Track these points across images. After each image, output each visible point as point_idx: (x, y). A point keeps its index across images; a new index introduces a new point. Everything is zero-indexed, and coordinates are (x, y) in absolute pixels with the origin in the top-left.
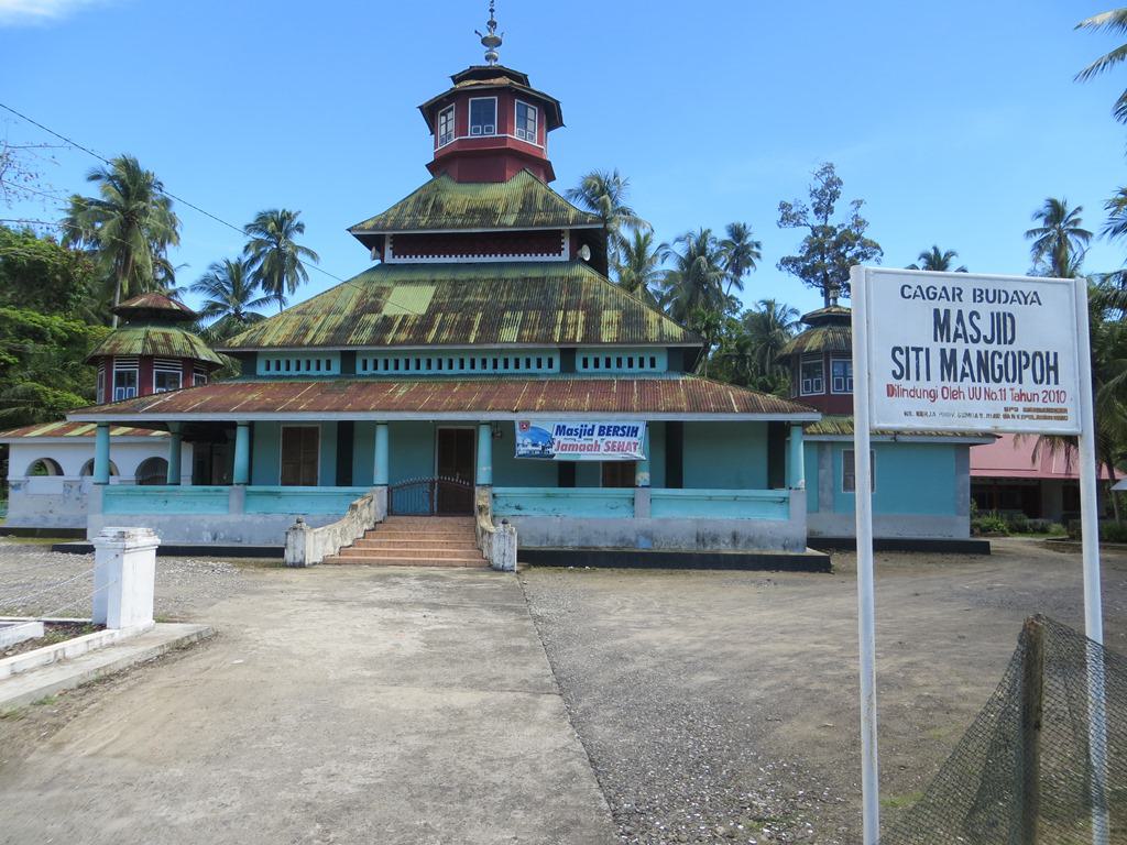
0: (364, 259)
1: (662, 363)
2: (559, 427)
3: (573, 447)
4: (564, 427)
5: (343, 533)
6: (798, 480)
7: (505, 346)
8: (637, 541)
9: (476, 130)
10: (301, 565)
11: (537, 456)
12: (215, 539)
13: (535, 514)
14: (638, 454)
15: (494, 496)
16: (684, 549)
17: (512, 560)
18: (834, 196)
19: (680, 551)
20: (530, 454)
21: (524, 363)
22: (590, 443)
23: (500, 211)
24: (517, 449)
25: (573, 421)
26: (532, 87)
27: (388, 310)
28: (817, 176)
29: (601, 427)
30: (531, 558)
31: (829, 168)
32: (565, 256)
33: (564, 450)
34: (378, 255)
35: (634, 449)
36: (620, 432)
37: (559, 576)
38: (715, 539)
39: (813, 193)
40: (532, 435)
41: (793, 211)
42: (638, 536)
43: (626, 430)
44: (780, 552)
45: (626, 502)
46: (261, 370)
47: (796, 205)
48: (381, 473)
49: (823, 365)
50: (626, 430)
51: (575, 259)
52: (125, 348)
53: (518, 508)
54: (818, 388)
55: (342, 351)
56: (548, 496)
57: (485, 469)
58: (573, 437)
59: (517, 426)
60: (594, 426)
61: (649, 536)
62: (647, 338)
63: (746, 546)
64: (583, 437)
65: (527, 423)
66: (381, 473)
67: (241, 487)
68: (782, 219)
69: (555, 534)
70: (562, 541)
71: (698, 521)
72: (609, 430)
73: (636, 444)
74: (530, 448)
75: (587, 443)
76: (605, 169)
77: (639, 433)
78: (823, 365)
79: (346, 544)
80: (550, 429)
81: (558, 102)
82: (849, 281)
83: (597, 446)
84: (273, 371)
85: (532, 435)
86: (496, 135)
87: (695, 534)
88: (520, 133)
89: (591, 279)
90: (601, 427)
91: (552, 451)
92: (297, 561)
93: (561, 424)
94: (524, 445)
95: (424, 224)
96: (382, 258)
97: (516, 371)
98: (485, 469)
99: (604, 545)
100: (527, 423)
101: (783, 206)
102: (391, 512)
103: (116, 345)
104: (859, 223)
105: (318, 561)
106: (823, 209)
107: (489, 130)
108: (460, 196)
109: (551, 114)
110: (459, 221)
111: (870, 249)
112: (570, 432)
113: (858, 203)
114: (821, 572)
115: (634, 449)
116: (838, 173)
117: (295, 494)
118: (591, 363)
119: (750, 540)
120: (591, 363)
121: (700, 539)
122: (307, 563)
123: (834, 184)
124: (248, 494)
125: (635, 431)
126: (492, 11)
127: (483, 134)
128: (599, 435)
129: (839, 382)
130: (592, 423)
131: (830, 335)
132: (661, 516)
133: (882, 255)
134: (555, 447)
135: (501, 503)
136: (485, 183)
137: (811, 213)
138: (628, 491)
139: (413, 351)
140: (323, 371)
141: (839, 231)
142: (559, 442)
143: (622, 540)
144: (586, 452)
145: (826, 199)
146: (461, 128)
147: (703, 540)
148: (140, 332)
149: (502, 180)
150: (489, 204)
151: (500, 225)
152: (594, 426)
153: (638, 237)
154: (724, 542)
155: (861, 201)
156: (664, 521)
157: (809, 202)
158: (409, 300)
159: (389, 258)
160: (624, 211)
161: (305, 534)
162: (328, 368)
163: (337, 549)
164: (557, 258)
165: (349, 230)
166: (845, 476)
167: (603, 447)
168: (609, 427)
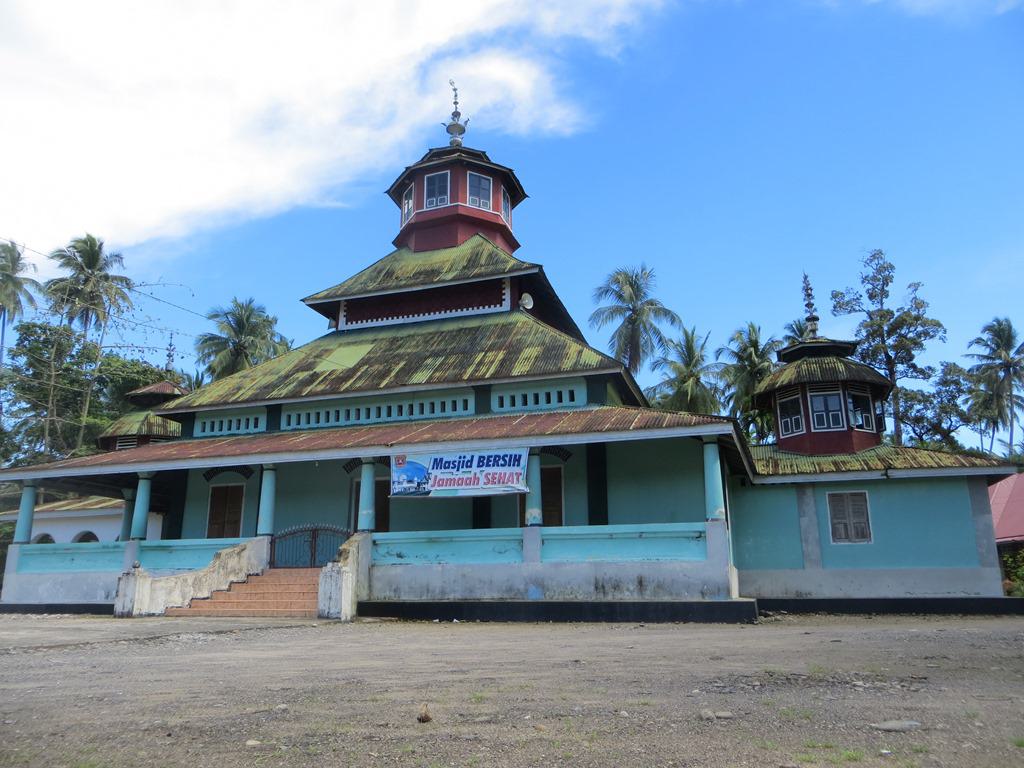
0: (321, 325)
1: (581, 394)
2: (436, 460)
3: (451, 481)
4: (441, 460)
5: (197, 583)
6: (716, 507)
7: (415, 389)
8: (527, 591)
9: (431, 203)
10: (129, 615)
11: (412, 493)
12: (107, 597)
13: (417, 563)
14: (520, 486)
15: (374, 542)
16: (581, 598)
17: (348, 609)
18: (887, 281)
19: (576, 601)
20: (405, 492)
21: (440, 405)
22: (469, 476)
23: (445, 271)
24: (392, 487)
25: (450, 452)
26: (492, 161)
27: (318, 369)
28: (867, 263)
29: (480, 457)
30: (368, 609)
31: (877, 255)
32: (506, 305)
33: (444, 486)
34: (334, 323)
35: (516, 481)
36: (501, 462)
37: (407, 624)
38: (617, 587)
39: (865, 280)
40: (408, 470)
41: (846, 299)
42: (527, 584)
43: (507, 459)
44: (697, 598)
45: (515, 545)
46: (197, 431)
47: (848, 292)
48: (265, 524)
49: (801, 401)
50: (507, 459)
51: (516, 306)
52: (123, 431)
53: (400, 556)
54: (798, 427)
55: (267, 406)
56: (431, 541)
57: (365, 512)
58: (450, 470)
59: (393, 462)
60: (473, 457)
61: (540, 584)
62: (560, 368)
63: (655, 593)
64: (461, 470)
65: (403, 458)
66: (265, 524)
67: (136, 541)
68: (835, 307)
69: (436, 583)
70: (443, 592)
71: (596, 564)
72: (489, 461)
73: (518, 475)
74: (406, 485)
75: (466, 476)
76: (631, 264)
77: (522, 461)
78: (801, 401)
79: (200, 595)
80: (426, 462)
81: (511, 170)
82: (914, 361)
83: (476, 480)
84: (208, 432)
85: (408, 470)
86: (449, 204)
87: (593, 581)
88: (474, 201)
89: (524, 323)
90: (480, 457)
91: (428, 487)
92: (126, 610)
93: (438, 457)
94: (400, 483)
95: (373, 289)
96: (337, 326)
97: (432, 416)
98: (365, 512)
99: (487, 596)
100: (403, 458)
101: (835, 295)
102: (272, 564)
103: (119, 428)
104: (919, 304)
105: (158, 612)
106: (878, 294)
107: (442, 201)
108: (413, 262)
109: (514, 192)
110: (404, 282)
111: (933, 328)
112: (447, 465)
113: (915, 286)
114: (742, 622)
115: (516, 481)
116: (889, 258)
117: (185, 548)
118: (507, 402)
119: (660, 586)
120: (507, 402)
121: (599, 587)
122: (134, 613)
123: (886, 269)
124: (143, 549)
125: (517, 459)
126: (456, 103)
127: (829, 427)
128: (479, 466)
129: (820, 418)
130: (471, 453)
131: (804, 367)
132: (554, 560)
133: (945, 332)
134: (431, 482)
135: (382, 550)
136: (438, 249)
137: (865, 299)
138: (517, 531)
139: (335, 401)
140: (252, 429)
141: (896, 314)
142: (436, 477)
143: (510, 589)
144: (464, 486)
145: (880, 281)
146: (419, 204)
147: (603, 587)
148: (141, 416)
149: (453, 244)
150: (436, 267)
151: (439, 282)
152: (473, 457)
153: (686, 333)
154: (628, 590)
155: (918, 284)
156: (557, 565)
157: (863, 289)
158: (345, 357)
159: (343, 325)
160: (651, 303)
161: (136, 580)
162: (256, 426)
163: (187, 602)
164: (498, 309)
165: (303, 300)
166: (833, 525)
167: (482, 480)
168: (489, 457)
